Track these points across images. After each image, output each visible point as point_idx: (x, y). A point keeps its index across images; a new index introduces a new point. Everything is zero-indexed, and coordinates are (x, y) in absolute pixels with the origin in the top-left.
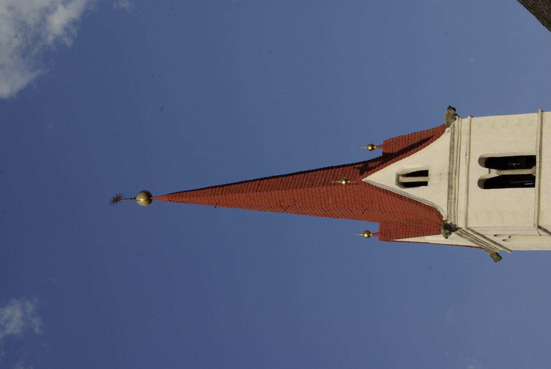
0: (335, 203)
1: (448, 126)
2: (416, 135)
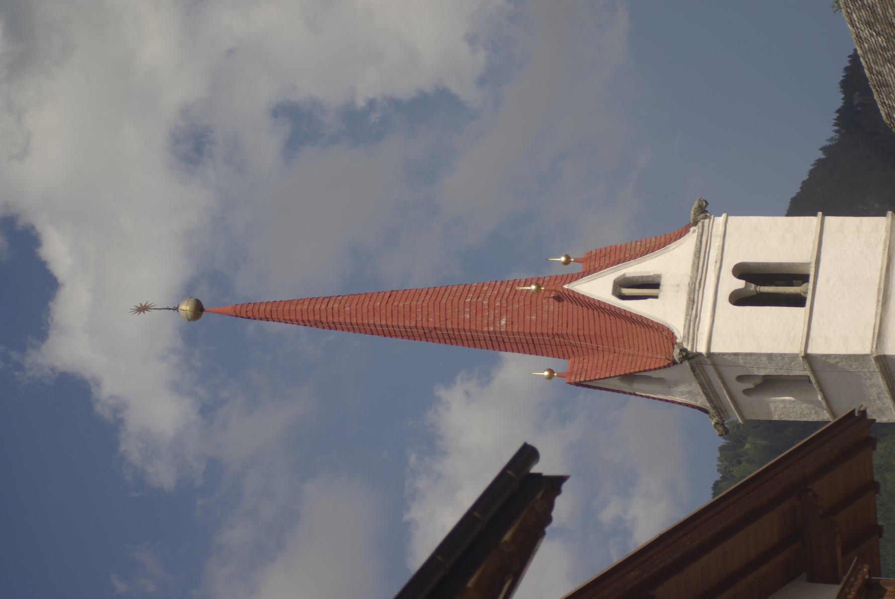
0: (511, 324)
1: (695, 223)
2: (639, 243)
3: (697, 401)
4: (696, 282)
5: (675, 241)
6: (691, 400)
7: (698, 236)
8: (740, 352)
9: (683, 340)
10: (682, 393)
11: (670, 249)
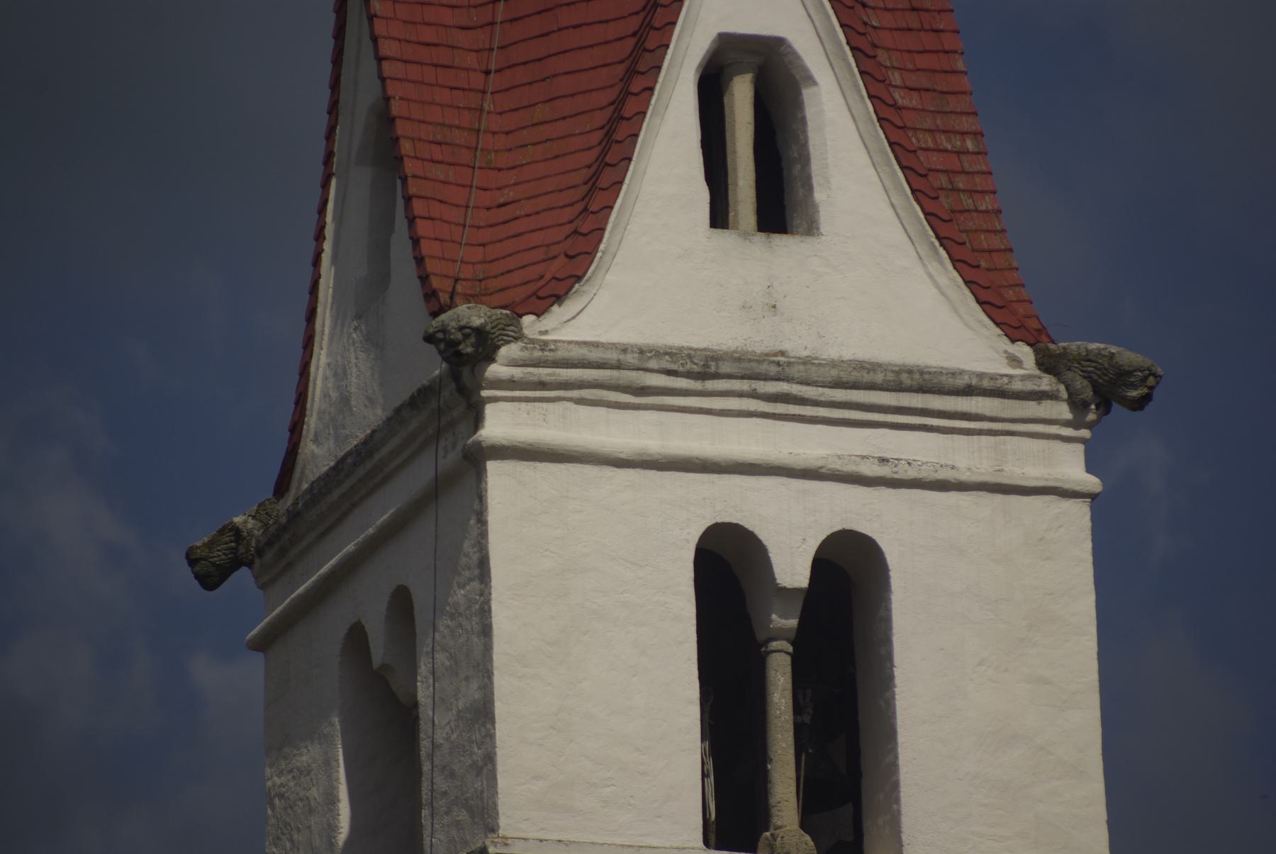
1: (1048, 363)
2: (970, 144)
3: (316, 440)
4: (788, 380)
5: (967, 283)
6: (321, 413)
7: (993, 377)
8: (493, 583)
9: (532, 341)
10: (340, 373)
11: (934, 267)
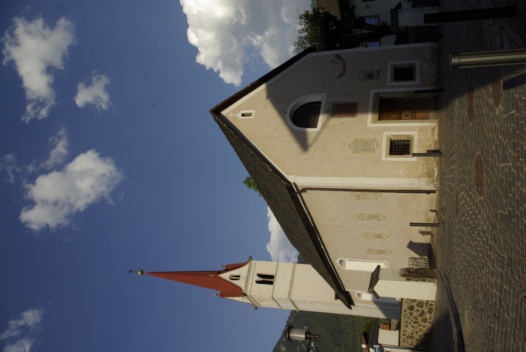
1: (249, 262)
